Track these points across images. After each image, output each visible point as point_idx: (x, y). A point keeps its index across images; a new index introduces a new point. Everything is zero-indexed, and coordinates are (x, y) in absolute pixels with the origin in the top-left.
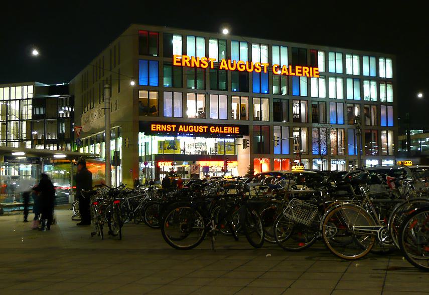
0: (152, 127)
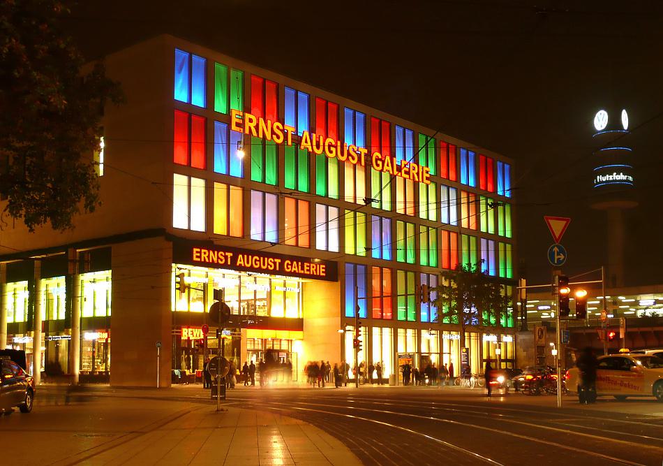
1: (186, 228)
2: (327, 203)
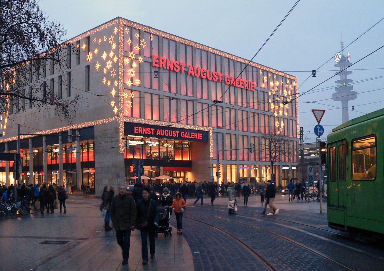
0: (135, 130)
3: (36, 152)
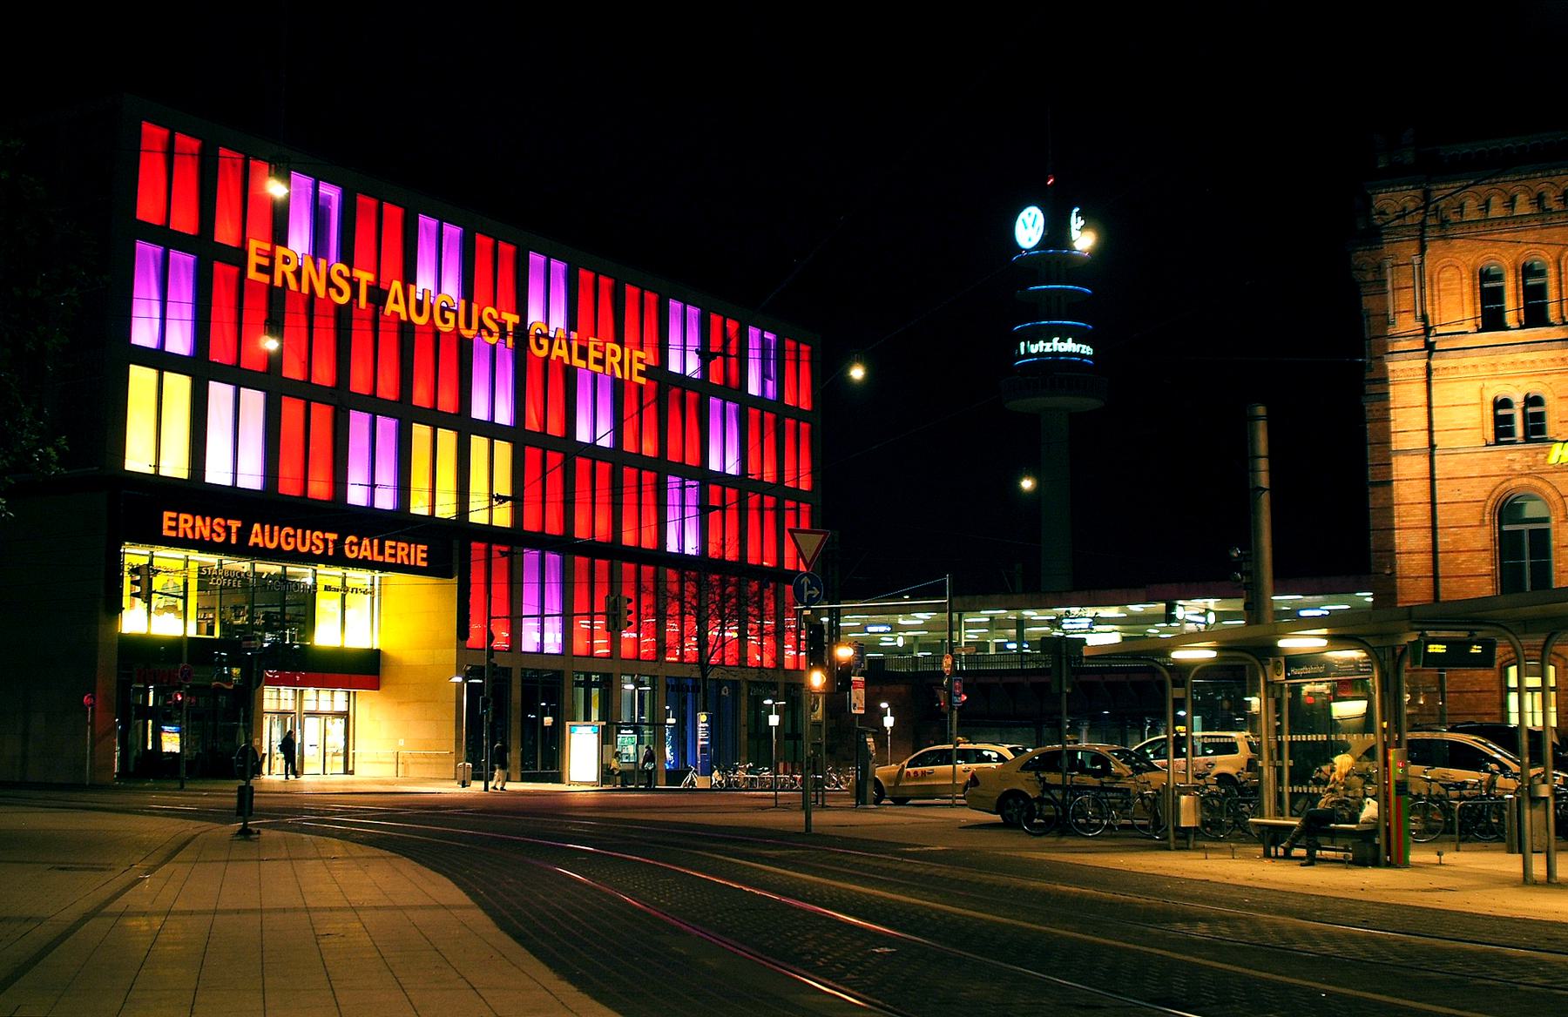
0: (166, 523)
1: (486, 522)
2: (593, 456)
3: (771, 619)
